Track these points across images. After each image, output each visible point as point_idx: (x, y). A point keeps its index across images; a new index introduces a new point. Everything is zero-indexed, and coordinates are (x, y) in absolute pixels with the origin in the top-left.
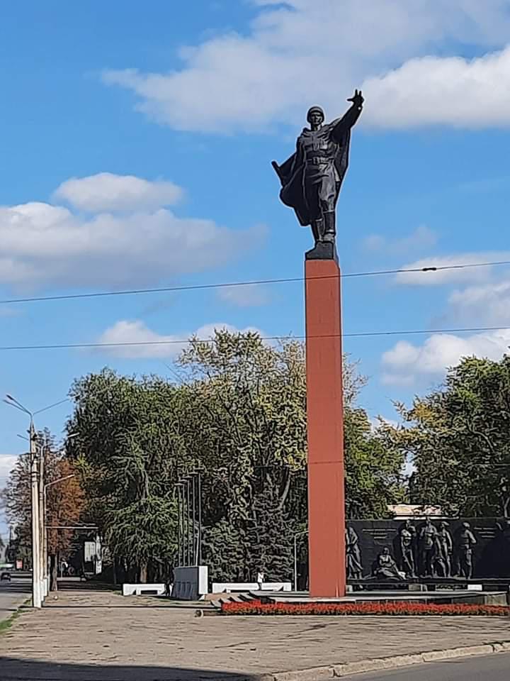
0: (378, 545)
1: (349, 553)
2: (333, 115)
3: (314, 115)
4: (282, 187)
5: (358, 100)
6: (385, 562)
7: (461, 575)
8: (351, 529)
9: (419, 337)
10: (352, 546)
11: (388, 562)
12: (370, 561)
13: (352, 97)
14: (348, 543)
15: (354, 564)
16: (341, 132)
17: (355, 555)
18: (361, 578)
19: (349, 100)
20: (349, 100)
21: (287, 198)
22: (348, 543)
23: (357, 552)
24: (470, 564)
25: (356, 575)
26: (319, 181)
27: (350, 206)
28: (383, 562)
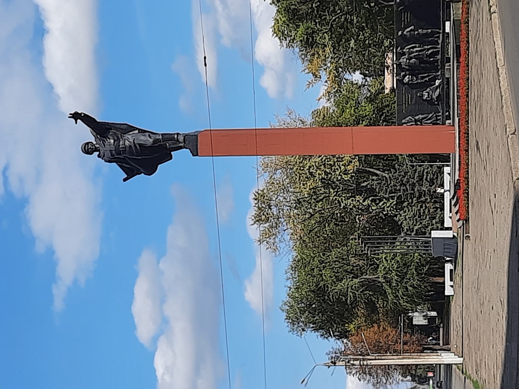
0: (415, 101)
1: (421, 123)
2: (87, 135)
3: (88, 149)
4: (143, 174)
5: (76, 116)
6: (428, 95)
7: (439, 37)
8: (403, 121)
9: (256, 69)
10: (416, 121)
11: (428, 93)
12: (428, 106)
13: (74, 121)
14: (414, 123)
15: (430, 119)
16: (101, 129)
17: (423, 119)
18: (440, 114)
19: (76, 123)
20: (76, 123)
21: (151, 170)
22: (414, 123)
23: (421, 116)
24: (429, 31)
25: (439, 118)
26: (138, 146)
27: (156, 121)
28: (428, 97)
